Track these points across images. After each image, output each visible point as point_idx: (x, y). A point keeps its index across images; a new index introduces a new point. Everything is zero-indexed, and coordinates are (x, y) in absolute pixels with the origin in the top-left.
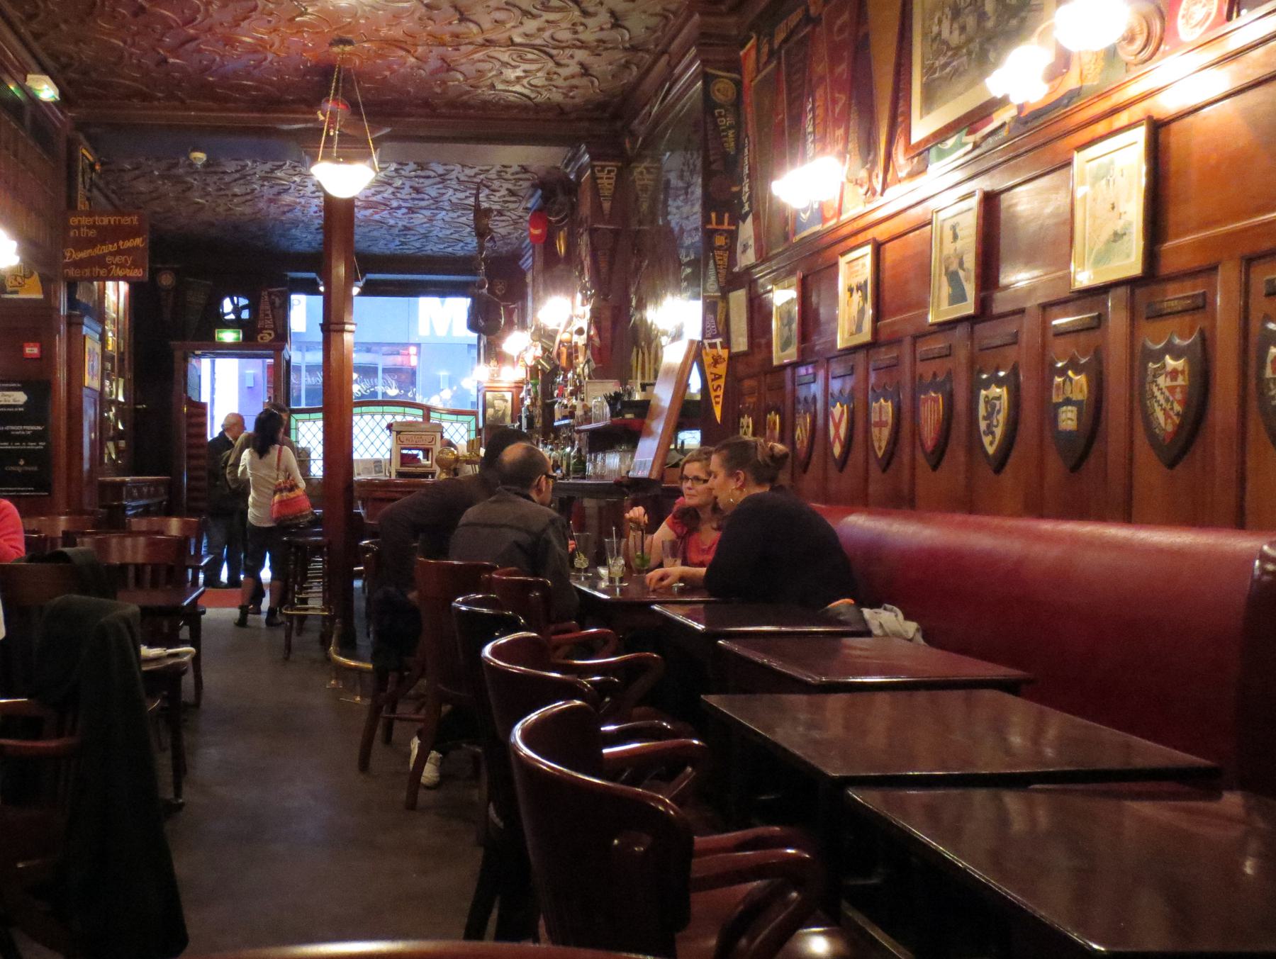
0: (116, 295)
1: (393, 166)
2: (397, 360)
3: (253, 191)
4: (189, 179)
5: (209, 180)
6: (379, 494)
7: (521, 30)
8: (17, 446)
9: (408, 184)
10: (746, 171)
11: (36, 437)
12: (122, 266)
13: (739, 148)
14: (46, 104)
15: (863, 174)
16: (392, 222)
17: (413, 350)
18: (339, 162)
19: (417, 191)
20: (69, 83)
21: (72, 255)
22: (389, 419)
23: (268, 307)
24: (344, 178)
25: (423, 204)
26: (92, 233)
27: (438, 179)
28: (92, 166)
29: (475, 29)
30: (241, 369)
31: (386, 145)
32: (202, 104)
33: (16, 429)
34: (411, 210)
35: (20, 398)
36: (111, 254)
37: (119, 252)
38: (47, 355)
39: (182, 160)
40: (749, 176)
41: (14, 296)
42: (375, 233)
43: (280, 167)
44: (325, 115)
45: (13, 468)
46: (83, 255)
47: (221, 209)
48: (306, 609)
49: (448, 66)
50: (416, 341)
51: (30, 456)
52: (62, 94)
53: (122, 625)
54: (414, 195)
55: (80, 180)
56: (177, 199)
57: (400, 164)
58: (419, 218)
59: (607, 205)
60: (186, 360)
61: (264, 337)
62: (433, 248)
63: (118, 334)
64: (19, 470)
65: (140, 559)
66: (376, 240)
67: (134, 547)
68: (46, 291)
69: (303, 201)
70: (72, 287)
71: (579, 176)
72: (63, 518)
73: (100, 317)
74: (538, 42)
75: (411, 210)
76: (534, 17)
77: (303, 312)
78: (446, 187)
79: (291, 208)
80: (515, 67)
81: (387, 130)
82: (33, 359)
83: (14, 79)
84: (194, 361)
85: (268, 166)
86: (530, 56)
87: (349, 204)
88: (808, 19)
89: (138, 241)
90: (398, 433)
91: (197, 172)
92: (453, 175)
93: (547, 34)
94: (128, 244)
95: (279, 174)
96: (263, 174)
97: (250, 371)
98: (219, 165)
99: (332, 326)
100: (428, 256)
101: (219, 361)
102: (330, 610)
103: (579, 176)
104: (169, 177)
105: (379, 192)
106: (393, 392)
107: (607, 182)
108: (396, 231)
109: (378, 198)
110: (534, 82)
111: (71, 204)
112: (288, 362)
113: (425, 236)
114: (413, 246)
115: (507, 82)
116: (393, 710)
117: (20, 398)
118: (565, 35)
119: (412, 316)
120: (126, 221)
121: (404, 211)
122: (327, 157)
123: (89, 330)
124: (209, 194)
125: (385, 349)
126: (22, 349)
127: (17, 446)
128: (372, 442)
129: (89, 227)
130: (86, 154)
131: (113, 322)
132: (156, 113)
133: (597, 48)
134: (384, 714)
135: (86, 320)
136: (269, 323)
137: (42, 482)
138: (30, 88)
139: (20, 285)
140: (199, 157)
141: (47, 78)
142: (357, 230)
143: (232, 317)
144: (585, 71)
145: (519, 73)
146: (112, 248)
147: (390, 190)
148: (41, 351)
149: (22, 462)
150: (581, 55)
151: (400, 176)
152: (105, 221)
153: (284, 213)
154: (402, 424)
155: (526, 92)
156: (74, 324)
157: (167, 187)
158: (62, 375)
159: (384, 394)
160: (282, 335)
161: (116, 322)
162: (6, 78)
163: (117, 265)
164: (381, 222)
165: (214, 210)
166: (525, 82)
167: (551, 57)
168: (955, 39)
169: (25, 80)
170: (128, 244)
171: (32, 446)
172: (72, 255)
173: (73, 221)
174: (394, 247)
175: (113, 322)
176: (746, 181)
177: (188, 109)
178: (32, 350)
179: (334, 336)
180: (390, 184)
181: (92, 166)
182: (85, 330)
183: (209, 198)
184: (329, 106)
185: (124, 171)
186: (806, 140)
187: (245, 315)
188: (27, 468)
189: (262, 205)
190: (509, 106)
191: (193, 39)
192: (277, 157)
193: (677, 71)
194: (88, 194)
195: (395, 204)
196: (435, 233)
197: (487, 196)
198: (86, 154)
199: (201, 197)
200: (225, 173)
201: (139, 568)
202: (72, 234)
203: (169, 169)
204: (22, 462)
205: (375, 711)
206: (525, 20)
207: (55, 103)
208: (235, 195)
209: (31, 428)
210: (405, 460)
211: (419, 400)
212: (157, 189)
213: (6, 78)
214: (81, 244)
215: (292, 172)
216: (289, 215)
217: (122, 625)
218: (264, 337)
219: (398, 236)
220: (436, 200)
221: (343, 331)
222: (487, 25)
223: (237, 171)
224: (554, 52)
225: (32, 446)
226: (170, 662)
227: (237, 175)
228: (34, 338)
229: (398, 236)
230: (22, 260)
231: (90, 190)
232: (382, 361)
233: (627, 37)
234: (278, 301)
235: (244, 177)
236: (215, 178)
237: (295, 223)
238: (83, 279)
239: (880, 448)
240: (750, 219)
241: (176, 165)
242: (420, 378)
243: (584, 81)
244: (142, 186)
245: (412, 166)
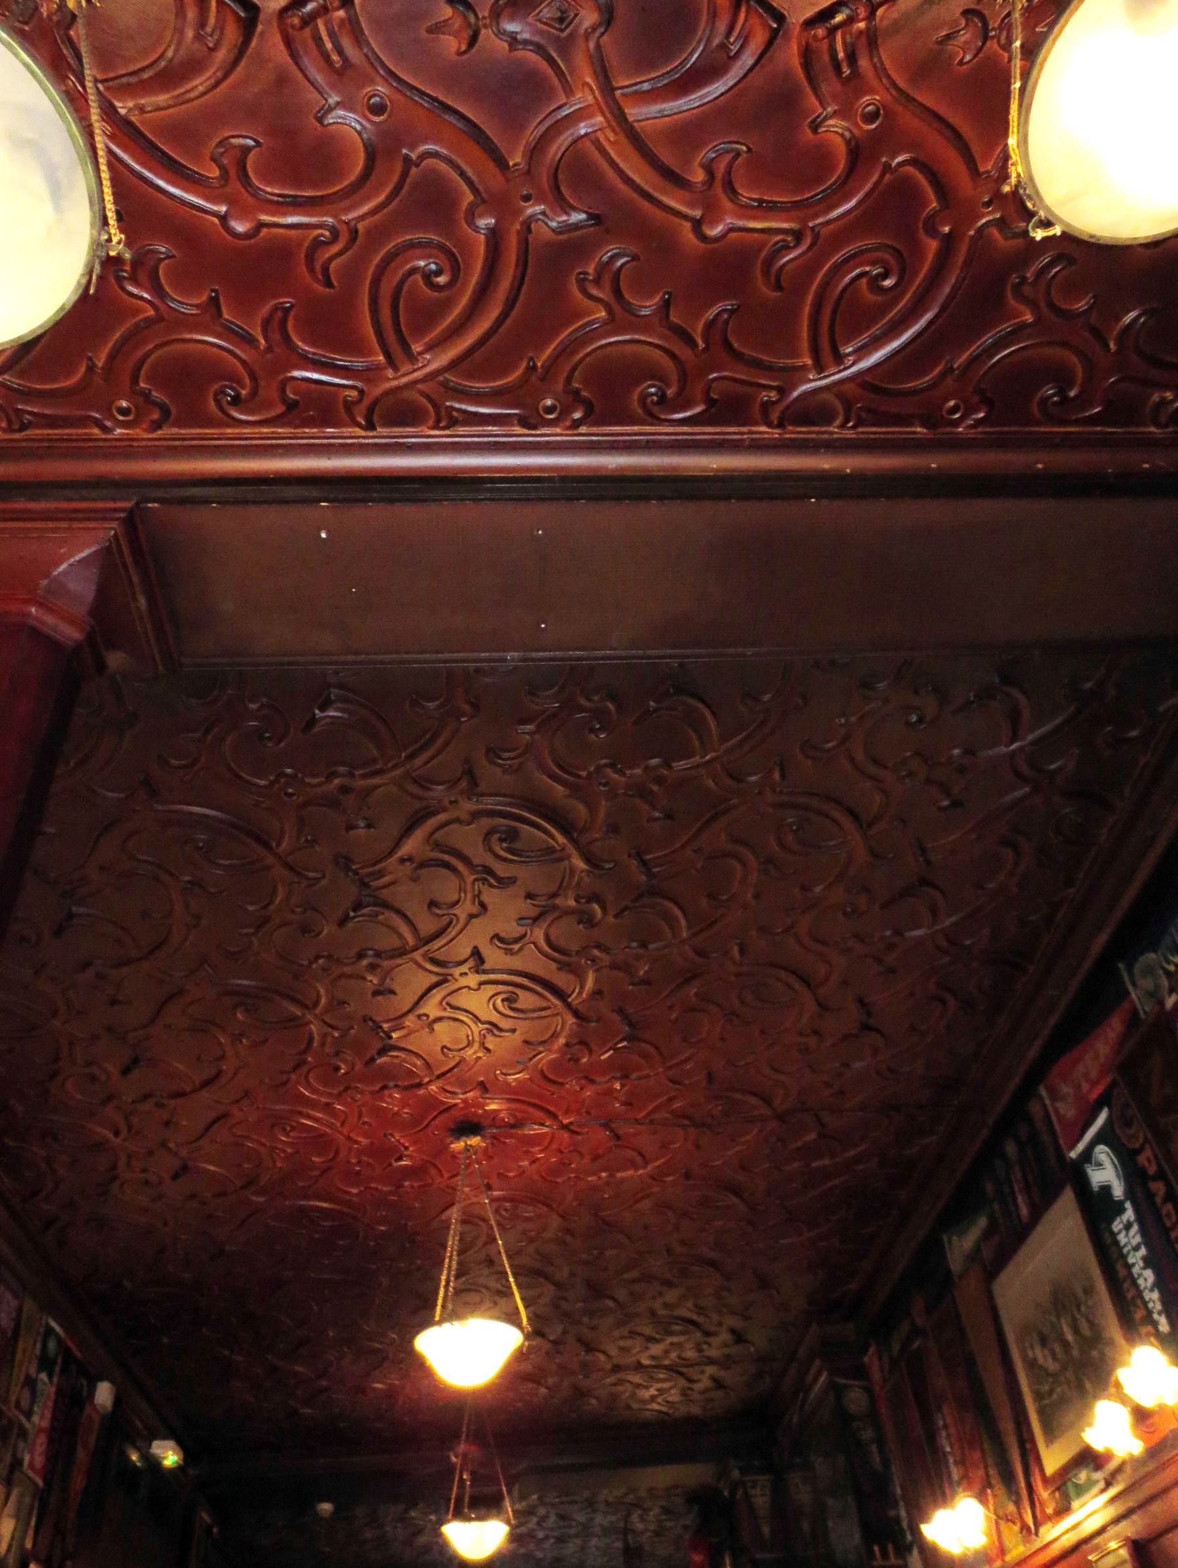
7: (647, 1353)
10: (899, 1491)
13: (886, 1464)
15: (1011, 1508)
18: (469, 1519)
25: (572, 1531)
29: (602, 1357)
34: (561, 1540)
40: (903, 1497)
44: (456, 1457)
49: (580, 1393)
54: (561, 1523)
58: (571, 1548)
59: (766, 1530)
71: (733, 1493)
74: (667, 1362)
76: (658, 1341)
80: (647, 1388)
86: (661, 1376)
88: (916, 1332)
92: (602, 1497)
93: (673, 1355)
103: (733, 1493)
107: (761, 1500)
110: (670, 1399)
115: (644, 1402)
118: (690, 1354)
133: (725, 1362)
141: (171, 1443)
144: (718, 1384)
145: (653, 1391)
147: (535, 1519)
150: (711, 1370)
155: (663, 1409)
166: (660, 1400)
167: (682, 1374)
168: (1052, 1366)
176: (902, 1504)
184: (462, 1448)
186: (947, 1462)
190: (646, 1425)
191: (327, 1389)
193: (809, 1378)
195: (541, 1535)
197: (641, 1517)
206: (650, 1345)
222: (613, 1351)
224: (685, 1370)
233: (752, 1349)
240: (915, 1552)
243: (718, 1394)
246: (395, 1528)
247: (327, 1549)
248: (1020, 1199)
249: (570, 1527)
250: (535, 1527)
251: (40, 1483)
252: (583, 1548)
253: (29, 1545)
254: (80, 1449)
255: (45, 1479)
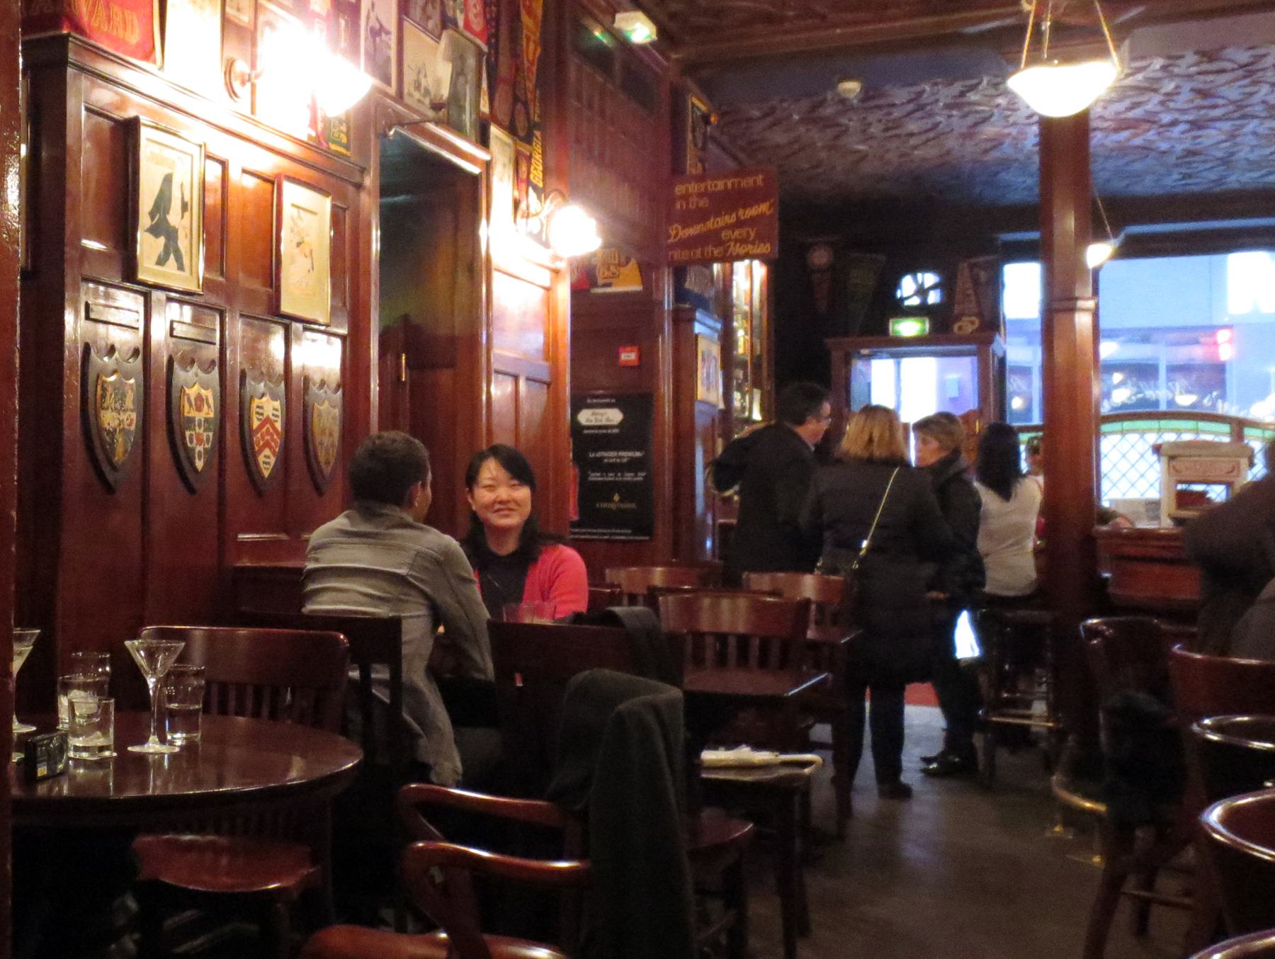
0: (748, 280)
1: (1158, 63)
2: (1197, 353)
3: (936, 125)
4: (844, 121)
5: (872, 118)
6: (1130, 550)
8: (610, 477)
9: (1187, 86)
11: (633, 465)
12: (743, 241)
14: (643, 48)
16: (1164, 146)
17: (1222, 336)
18: (1052, 65)
19: (1203, 94)
20: (673, 16)
21: (679, 232)
22: (1152, 438)
23: (969, 285)
24: (1054, 88)
26: (704, 203)
27: (1241, 72)
28: (706, 119)
30: (942, 371)
31: (1139, 32)
32: (850, 16)
33: (610, 456)
34: (1196, 125)
35: (614, 416)
36: (727, 227)
37: (740, 224)
38: (647, 365)
39: (829, 95)
41: (608, 290)
42: (1138, 166)
43: (973, 88)
45: (605, 505)
46: (692, 231)
47: (892, 156)
48: (1029, 717)
50: (1226, 320)
51: (628, 491)
52: (662, 31)
53: (650, 718)
54: (1199, 102)
55: (690, 136)
56: (831, 148)
57: (1170, 57)
58: (1211, 136)
60: (847, 363)
61: (965, 324)
62: (1238, 179)
63: (752, 332)
64: (613, 506)
65: (741, 628)
66: (1139, 176)
67: (734, 611)
68: (645, 280)
69: (1014, 131)
70: (679, 274)
72: (659, 569)
73: (725, 310)
75: (1196, 125)
77: (1022, 288)
78: (1255, 83)
79: (996, 142)
81: (1134, 12)
82: (629, 367)
83: (597, 20)
84: (858, 365)
85: (958, 87)
87: (1080, 126)
89: (763, 208)
90: (1172, 458)
91: (852, 108)
94: (752, 212)
95: (973, 97)
96: (949, 101)
97: (953, 376)
98: (882, 95)
99: (1058, 303)
100: (1234, 191)
101: (906, 362)
102: (1056, 721)
104: (815, 121)
105: (1135, 105)
106: (1185, 400)
108: (1172, 159)
109: (1137, 113)
111: (677, 170)
112: (1002, 361)
113: (1226, 161)
114: (1205, 178)
116: (1149, 884)
117: (614, 416)
119: (1215, 285)
120: (747, 183)
121: (1182, 127)
122: (1034, 60)
123: (704, 328)
124: (872, 137)
125: (1172, 336)
126: (617, 356)
127: (610, 477)
128: (1130, 475)
129: (701, 195)
130: (697, 104)
131: (745, 316)
132: (789, 37)
134: (1130, 886)
135: (698, 315)
136: (972, 306)
137: (642, 524)
138: (619, 31)
139: (614, 276)
140: (851, 88)
141: (640, 15)
142: (1095, 166)
143: (915, 301)
146: (730, 219)
147: (1157, 98)
148: (640, 357)
149: (616, 498)
151: (1173, 76)
152: (720, 185)
153: (986, 151)
154: (1176, 445)
156: (682, 321)
157: (819, 137)
158: (666, 389)
159: (1171, 402)
160: (991, 323)
161: (750, 316)
162: (588, 22)
163: (736, 241)
164: (1146, 149)
165: (881, 158)
169: (613, 22)
170: (752, 212)
171: (629, 477)
172: (679, 232)
173: (679, 189)
174: (1172, 182)
175: (745, 316)
177: (835, 26)
178: (629, 356)
179: (1060, 319)
180: (1155, 91)
181: (706, 119)
182: (698, 328)
183: (874, 143)
185: (750, 120)
187: (934, 298)
188: (623, 506)
189: (951, 143)
192: (966, 73)
194: (700, 153)
195: (1166, 118)
196: (1242, 155)
198: (697, 104)
199: (864, 141)
200: (894, 105)
201: (743, 640)
202: (678, 206)
203: (814, 108)
204: (616, 498)
205: (1113, 883)
207: (653, 44)
208: (911, 135)
209: (626, 455)
210: (1184, 499)
211: (1223, 408)
212: (797, 140)
213: (588, 22)
214: (688, 218)
215: (992, 91)
216: (995, 154)
217: (650, 718)
218: (965, 324)
219: (1177, 165)
220: (1239, 105)
221: (1073, 310)
223: (909, 102)
225: (629, 477)
226: (784, 772)
227: (911, 107)
228: (631, 340)
229: (1177, 165)
230: (606, 246)
231: (704, 148)
232: (1163, 355)
234: (983, 276)
235: (921, 108)
236: (879, 114)
237: (1005, 164)
238: (692, 262)
239: (327, 463)
241: (822, 103)
242: (1232, 379)
244: (779, 137)
245: (1191, 58)
246: (950, 116)
247: (861, 147)
248: (673, 801)
249: (1215, 107)
250: (1159, 108)
251: (485, 48)
252: (1232, 136)
253: (485, 108)
254: (525, 18)
255: (488, 43)
